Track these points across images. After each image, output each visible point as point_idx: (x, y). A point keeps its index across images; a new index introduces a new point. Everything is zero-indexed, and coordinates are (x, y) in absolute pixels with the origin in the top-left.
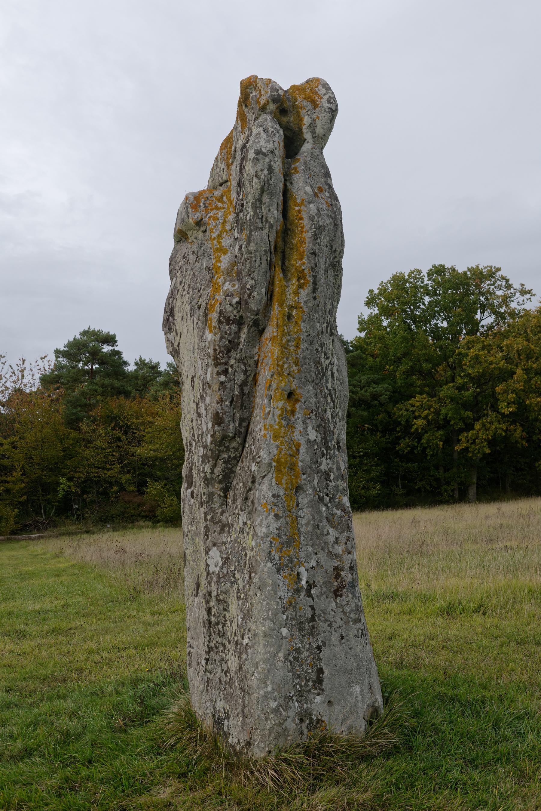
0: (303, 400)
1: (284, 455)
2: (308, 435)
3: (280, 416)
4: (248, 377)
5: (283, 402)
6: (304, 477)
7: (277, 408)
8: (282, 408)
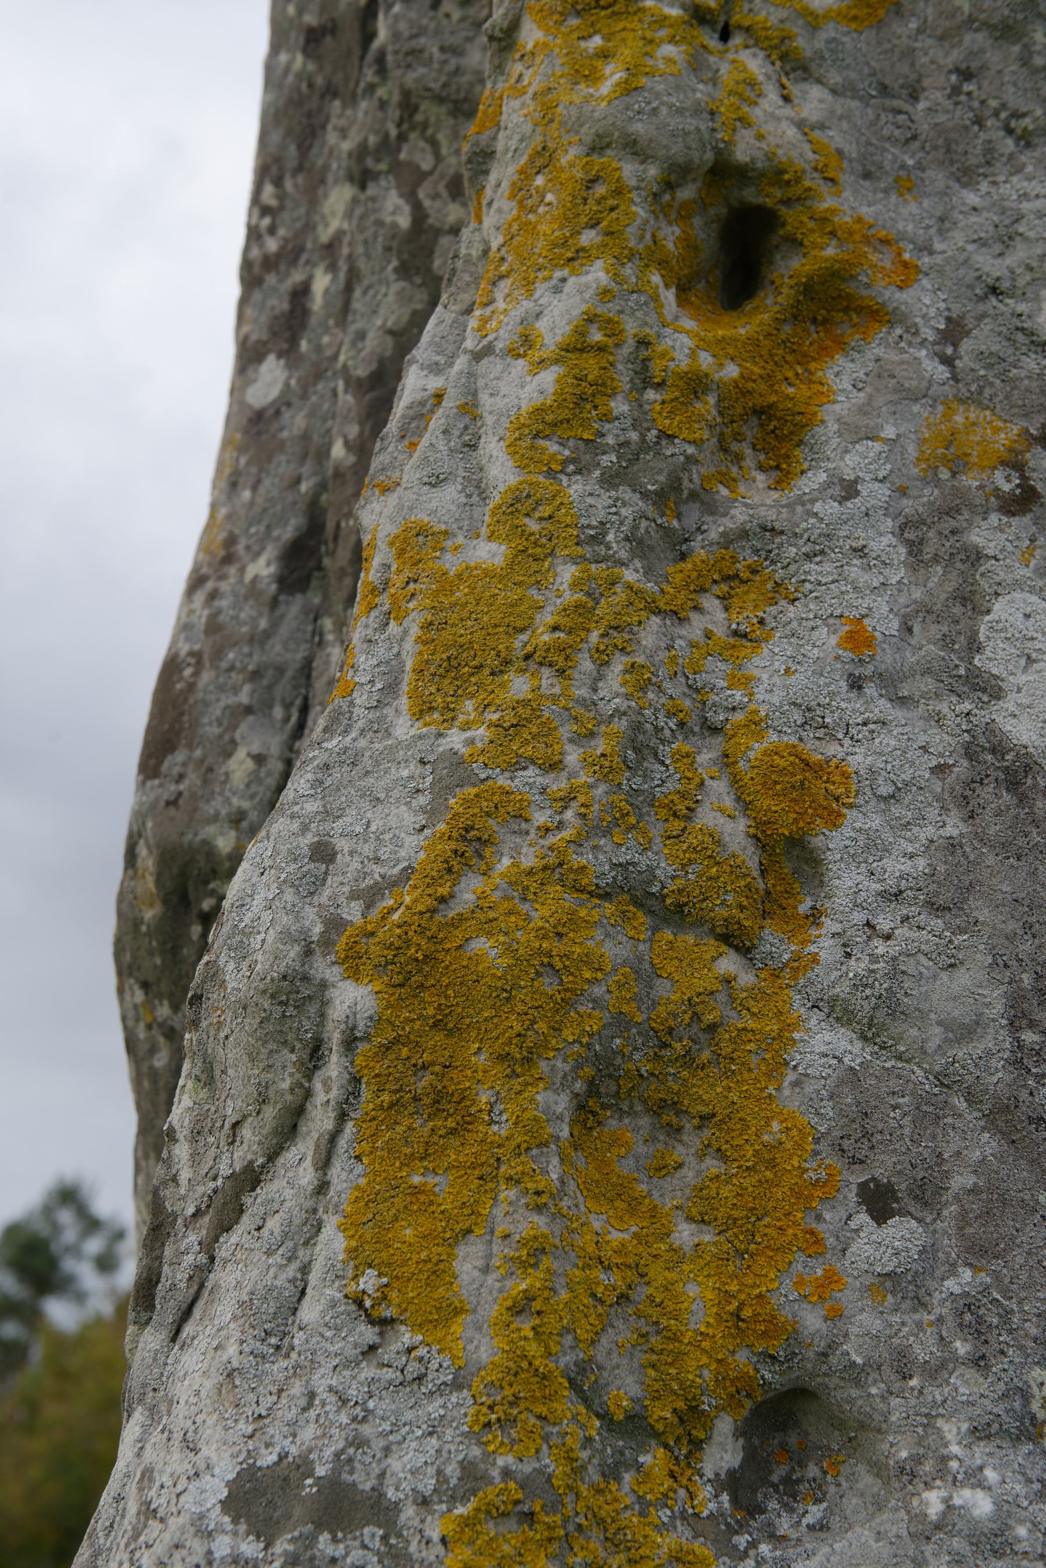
0: (925, 303)
1: (526, 885)
2: (988, 688)
3: (541, 424)
5: (598, 274)
6: (880, 1245)
7: (525, 343)
8: (576, 347)
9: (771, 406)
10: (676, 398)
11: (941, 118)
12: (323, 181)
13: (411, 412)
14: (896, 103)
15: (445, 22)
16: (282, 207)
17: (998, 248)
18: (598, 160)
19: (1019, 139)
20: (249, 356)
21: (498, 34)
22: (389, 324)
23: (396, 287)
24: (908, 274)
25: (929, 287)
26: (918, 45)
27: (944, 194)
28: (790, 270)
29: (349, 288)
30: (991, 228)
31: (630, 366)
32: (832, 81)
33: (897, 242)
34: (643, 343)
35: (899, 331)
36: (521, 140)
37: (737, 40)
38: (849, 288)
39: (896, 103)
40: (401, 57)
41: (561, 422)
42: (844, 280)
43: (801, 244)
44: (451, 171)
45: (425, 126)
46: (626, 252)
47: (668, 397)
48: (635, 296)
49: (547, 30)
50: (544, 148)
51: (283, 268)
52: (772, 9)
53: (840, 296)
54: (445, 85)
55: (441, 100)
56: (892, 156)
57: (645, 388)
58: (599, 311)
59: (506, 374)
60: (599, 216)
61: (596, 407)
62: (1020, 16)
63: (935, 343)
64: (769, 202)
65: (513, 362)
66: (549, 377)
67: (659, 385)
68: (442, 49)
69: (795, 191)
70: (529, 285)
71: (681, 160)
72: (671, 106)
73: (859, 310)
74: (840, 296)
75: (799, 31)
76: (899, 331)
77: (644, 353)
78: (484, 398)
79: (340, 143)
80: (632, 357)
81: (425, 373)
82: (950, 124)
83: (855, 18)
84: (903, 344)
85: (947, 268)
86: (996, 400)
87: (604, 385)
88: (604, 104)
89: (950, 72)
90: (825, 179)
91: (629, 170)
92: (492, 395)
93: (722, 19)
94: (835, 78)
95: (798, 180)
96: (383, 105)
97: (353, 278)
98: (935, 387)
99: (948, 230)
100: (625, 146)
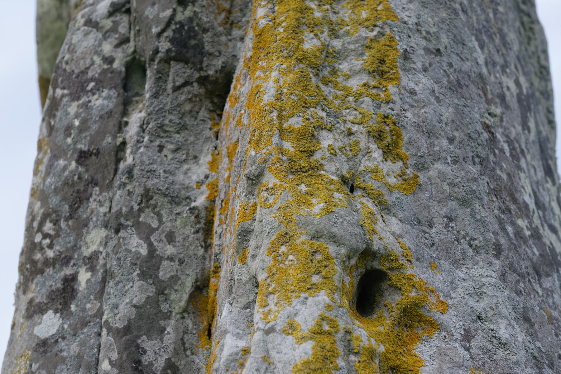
4: (162, 290)
7: (291, 328)
8: (318, 332)
9: (398, 366)
10: (365, 360)
11: (443, 237)
12: (86, 225)
13: (231, 358)
14: (424, 228)
15: (165, 159)
16: (58, 235)
17: (476, 298)
18: (317, 243)
19: (474, 249)
20: (33, 311)
21: (252, 177)
22: (134, 302)
23: (138, 284)
24: (444, 307)
25: (453, 313)
26: (431, 204)
27: (450, 271)
28: (394, 301)
29: (104, 281)
30: (472, 289)
31: (342, 343)
32: (400, 216)
33: (436, 292)
34: (348, 332)
35: (444, 334)
36: (272, 229)
37: (358, 193)
38: (421, 311)
39: (424, 228)
40: (144, 173)
41: (318, 369)
42: (419, 308)
43: (400, 289)
44: (168, 229)
45: (155, 206)
46: (334, 287)
47: (362, 360)
48: (341, 309)
49: (281, 180)
50: (286, 234)
51: (57, 266)
52: (373, 181)
53: (417, 315)
54: (167, 189)
55: (165, 195)
56: (427, 252)
57: (349, 354)
58: (327, 315)
59: (283, 343)
60: (320, 269)
61: (332, 363)
62: (470, 197)
63: (461, 341)
64: (384, 269)
65: (286, 337)
66: (308, 346)
67: (356, 353)
68: (165, 171)
69: (394, 265)
70: (288, 299)
71: (355, 247)
72: (348, 222)
73: (425, 322)
74: (417, 315)
75: (385, 192)
76: (444, 334)
77: (348, 337)
78: (273, 353)
79: (97, 206)
80: (343, 338)
81: (235, 338)
82: (447, 240)
83: (405, 189)
84: (446, 340)
85: (459, 306)
86: (492, 370)
87: (333, 351)
88: (318, 217)
89: (444, 217)
90: (407, 260)
91: (332, 249)
92: (278, 353)
93: (351, 182)
94: (401, 215)
95: (397, 260)
96: (130, 193)
97: (107, 275)
98: (466, 362)
99: (455, 288)
100: (330, 238)
